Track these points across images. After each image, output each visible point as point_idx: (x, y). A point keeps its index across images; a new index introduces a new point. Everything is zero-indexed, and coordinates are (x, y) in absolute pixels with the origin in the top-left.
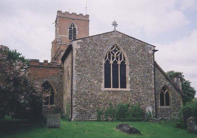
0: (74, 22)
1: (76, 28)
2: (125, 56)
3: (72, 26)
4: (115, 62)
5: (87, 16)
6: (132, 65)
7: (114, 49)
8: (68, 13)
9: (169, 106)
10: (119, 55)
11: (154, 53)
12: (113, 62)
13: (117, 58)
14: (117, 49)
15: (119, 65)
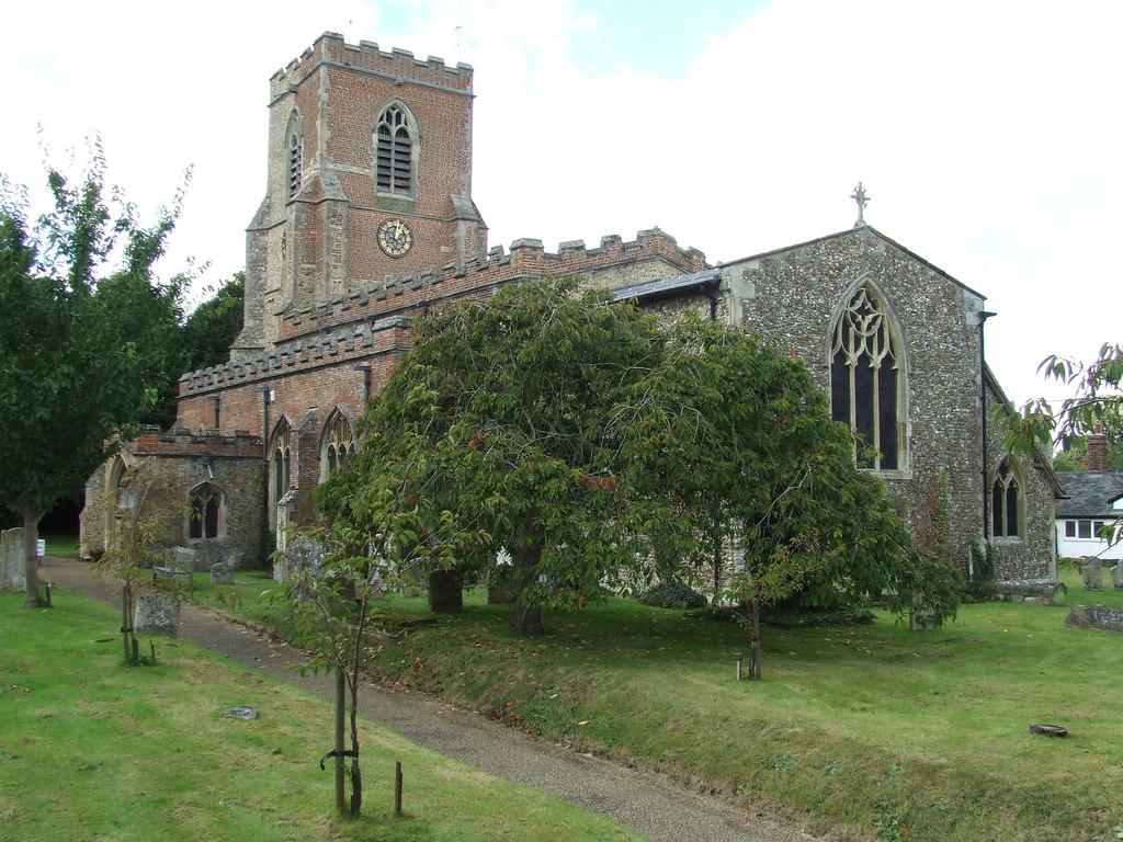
0: (397, 99)
1: (412, 129)
2: (894, 335)
3: (389, 120)
4: (864, 359)
5: (464, 74)
6: (917, 372)
7: (859, 304)
8: (374, 48)
9: (1016, 534)
10: (875, 329)
11: (981, 326)
12: (883, 361)
13: (870, 341)
14: (869, 305)
15: (876, 374)
